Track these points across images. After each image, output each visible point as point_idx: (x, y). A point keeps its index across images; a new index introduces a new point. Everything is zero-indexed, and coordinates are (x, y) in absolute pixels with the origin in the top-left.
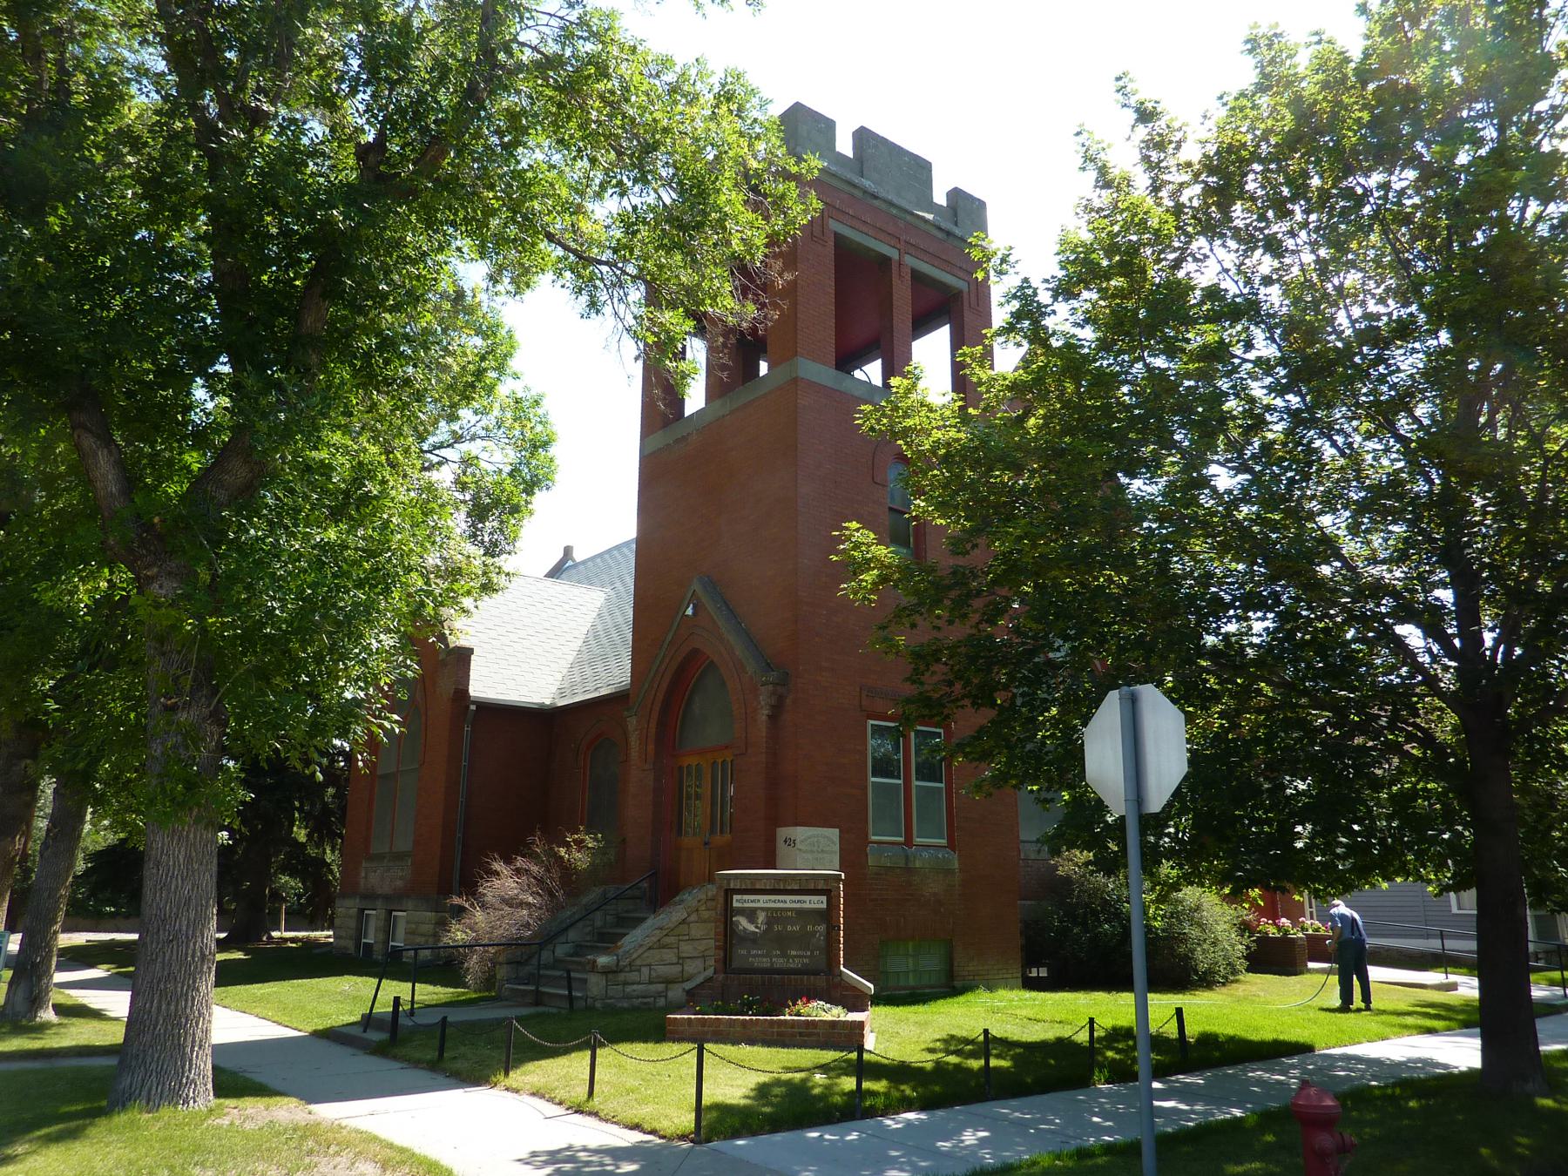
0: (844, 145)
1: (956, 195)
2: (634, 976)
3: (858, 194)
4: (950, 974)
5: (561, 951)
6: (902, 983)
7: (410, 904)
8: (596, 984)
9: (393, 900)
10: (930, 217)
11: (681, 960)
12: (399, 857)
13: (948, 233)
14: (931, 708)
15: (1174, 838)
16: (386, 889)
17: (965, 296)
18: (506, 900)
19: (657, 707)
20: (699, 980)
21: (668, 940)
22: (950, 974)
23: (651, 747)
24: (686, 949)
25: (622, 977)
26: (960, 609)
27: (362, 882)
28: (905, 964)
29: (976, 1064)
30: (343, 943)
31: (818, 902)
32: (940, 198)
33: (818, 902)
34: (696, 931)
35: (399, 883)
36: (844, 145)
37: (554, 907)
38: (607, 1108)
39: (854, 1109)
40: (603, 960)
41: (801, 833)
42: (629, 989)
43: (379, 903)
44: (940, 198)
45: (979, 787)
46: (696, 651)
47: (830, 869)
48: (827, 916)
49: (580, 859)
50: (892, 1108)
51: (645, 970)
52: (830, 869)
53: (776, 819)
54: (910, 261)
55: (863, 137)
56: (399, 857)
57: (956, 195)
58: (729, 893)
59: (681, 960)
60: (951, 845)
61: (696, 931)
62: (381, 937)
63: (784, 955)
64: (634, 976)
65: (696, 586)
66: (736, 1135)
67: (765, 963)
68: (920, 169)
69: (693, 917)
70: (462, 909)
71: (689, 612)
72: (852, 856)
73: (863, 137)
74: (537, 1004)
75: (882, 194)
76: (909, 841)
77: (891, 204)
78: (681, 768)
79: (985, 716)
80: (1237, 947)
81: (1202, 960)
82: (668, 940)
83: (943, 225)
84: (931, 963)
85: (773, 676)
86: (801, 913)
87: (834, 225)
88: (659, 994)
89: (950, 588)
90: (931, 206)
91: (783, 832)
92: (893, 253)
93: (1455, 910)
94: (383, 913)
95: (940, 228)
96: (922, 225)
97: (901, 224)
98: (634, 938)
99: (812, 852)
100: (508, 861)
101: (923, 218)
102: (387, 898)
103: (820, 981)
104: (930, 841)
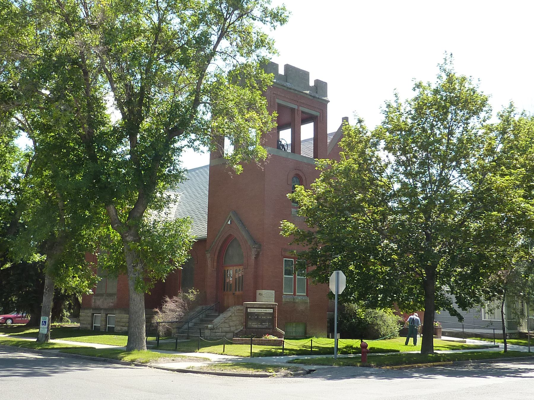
0: (281, 71)
1: (317, 82)
2: (217, 331)
3: (285, 89)
4: (306, 333)
5: (191, 325)
6: (291, 335)
7: (117, 312)
8: (207, 333)
9: (108, 310)
10: (308, 92)
11: (230, 326)
12: (110, 295)
13: (314, 97)
14: (302, 266)
15: (353, 297)
16: (105, 306)
17: (319, 117)
18: (171, 311)
19: (217, 251)
20: (239, 330)
21: (227, 321)
22: (306, 333)
23: (215, 264)
24: (231, 324)
25: (214, 331)
26: (310, 241)
27: (93, 304)
28: (293, 329)
29: (310, 349)
30: (84, 326)
31: (271, 311)
32: (312, 83)
33: (271, 311)
34: (234, 318)
35: (111, 304)
36: (281, 71)
37: (186, 313)
38: (228, 353)
39: (281, 354)
40: (209, 326)
41: (264, 292)
42: (216, 334)
43: (102, 311)
44: (312, 83)
45: (314, 282)
46: (231, 235)
47: (272, 301)
48: (272, 314)
49: (191, 297)
50: (290, 354)
51: (221, 329)
52: (272, 301)
53: (256, 288)
54: (301, 109)
55: (288, 68)
56: (110, 295)
57: (317, 82)
58: (247, 308)
59: (230, 326)
60: (307, 295)
61: (234, 318)
62: (104, 323)
63: (261, 324)
64: (217, 331)
65: (231, 214)
66: (258, 357)
67: (256, 326)
68: (305, 75)
69: (233, 315)
70: (157, 312)
71: (229, 223)
72: (278, 298)
73: (288, 68)
74: (188, 339)
75: (293, 88)
76: (295, 294)
77: (296, 90)
78: (225, 270)
79: (315, 268)
80: (397, 329)
81: (383, 331)
82: (227, 321)
83: (312, 94)
84: (300, 329)
85: (256, 246)
86: (266, 314)
87: (277, 101)
88: (224, 336)
89: (307, 237)
90: (308, 88)
91: (258, 292)
92: (295, 107)
93: (483, 319)
94: (104, 315)
95: (311, 96)
96: (305, 95)
97: (298, 96)
98: (216, 321)
99: (267, 297)
100: (171, 297)
101: (306, 93)
102: (105, 309)
103: (271, 331)
104: (301, 294)
